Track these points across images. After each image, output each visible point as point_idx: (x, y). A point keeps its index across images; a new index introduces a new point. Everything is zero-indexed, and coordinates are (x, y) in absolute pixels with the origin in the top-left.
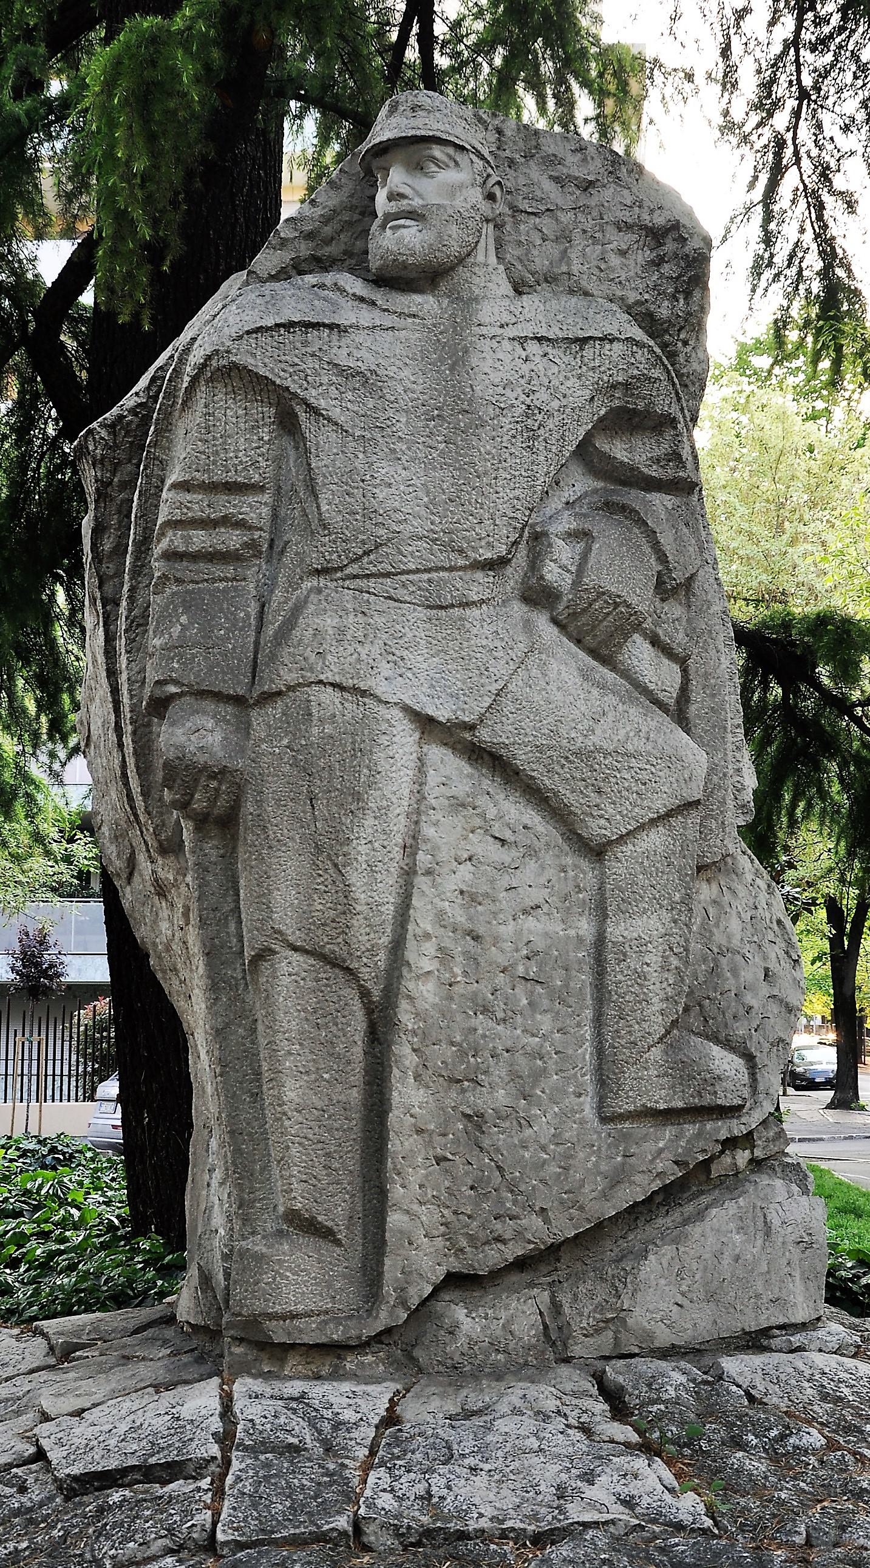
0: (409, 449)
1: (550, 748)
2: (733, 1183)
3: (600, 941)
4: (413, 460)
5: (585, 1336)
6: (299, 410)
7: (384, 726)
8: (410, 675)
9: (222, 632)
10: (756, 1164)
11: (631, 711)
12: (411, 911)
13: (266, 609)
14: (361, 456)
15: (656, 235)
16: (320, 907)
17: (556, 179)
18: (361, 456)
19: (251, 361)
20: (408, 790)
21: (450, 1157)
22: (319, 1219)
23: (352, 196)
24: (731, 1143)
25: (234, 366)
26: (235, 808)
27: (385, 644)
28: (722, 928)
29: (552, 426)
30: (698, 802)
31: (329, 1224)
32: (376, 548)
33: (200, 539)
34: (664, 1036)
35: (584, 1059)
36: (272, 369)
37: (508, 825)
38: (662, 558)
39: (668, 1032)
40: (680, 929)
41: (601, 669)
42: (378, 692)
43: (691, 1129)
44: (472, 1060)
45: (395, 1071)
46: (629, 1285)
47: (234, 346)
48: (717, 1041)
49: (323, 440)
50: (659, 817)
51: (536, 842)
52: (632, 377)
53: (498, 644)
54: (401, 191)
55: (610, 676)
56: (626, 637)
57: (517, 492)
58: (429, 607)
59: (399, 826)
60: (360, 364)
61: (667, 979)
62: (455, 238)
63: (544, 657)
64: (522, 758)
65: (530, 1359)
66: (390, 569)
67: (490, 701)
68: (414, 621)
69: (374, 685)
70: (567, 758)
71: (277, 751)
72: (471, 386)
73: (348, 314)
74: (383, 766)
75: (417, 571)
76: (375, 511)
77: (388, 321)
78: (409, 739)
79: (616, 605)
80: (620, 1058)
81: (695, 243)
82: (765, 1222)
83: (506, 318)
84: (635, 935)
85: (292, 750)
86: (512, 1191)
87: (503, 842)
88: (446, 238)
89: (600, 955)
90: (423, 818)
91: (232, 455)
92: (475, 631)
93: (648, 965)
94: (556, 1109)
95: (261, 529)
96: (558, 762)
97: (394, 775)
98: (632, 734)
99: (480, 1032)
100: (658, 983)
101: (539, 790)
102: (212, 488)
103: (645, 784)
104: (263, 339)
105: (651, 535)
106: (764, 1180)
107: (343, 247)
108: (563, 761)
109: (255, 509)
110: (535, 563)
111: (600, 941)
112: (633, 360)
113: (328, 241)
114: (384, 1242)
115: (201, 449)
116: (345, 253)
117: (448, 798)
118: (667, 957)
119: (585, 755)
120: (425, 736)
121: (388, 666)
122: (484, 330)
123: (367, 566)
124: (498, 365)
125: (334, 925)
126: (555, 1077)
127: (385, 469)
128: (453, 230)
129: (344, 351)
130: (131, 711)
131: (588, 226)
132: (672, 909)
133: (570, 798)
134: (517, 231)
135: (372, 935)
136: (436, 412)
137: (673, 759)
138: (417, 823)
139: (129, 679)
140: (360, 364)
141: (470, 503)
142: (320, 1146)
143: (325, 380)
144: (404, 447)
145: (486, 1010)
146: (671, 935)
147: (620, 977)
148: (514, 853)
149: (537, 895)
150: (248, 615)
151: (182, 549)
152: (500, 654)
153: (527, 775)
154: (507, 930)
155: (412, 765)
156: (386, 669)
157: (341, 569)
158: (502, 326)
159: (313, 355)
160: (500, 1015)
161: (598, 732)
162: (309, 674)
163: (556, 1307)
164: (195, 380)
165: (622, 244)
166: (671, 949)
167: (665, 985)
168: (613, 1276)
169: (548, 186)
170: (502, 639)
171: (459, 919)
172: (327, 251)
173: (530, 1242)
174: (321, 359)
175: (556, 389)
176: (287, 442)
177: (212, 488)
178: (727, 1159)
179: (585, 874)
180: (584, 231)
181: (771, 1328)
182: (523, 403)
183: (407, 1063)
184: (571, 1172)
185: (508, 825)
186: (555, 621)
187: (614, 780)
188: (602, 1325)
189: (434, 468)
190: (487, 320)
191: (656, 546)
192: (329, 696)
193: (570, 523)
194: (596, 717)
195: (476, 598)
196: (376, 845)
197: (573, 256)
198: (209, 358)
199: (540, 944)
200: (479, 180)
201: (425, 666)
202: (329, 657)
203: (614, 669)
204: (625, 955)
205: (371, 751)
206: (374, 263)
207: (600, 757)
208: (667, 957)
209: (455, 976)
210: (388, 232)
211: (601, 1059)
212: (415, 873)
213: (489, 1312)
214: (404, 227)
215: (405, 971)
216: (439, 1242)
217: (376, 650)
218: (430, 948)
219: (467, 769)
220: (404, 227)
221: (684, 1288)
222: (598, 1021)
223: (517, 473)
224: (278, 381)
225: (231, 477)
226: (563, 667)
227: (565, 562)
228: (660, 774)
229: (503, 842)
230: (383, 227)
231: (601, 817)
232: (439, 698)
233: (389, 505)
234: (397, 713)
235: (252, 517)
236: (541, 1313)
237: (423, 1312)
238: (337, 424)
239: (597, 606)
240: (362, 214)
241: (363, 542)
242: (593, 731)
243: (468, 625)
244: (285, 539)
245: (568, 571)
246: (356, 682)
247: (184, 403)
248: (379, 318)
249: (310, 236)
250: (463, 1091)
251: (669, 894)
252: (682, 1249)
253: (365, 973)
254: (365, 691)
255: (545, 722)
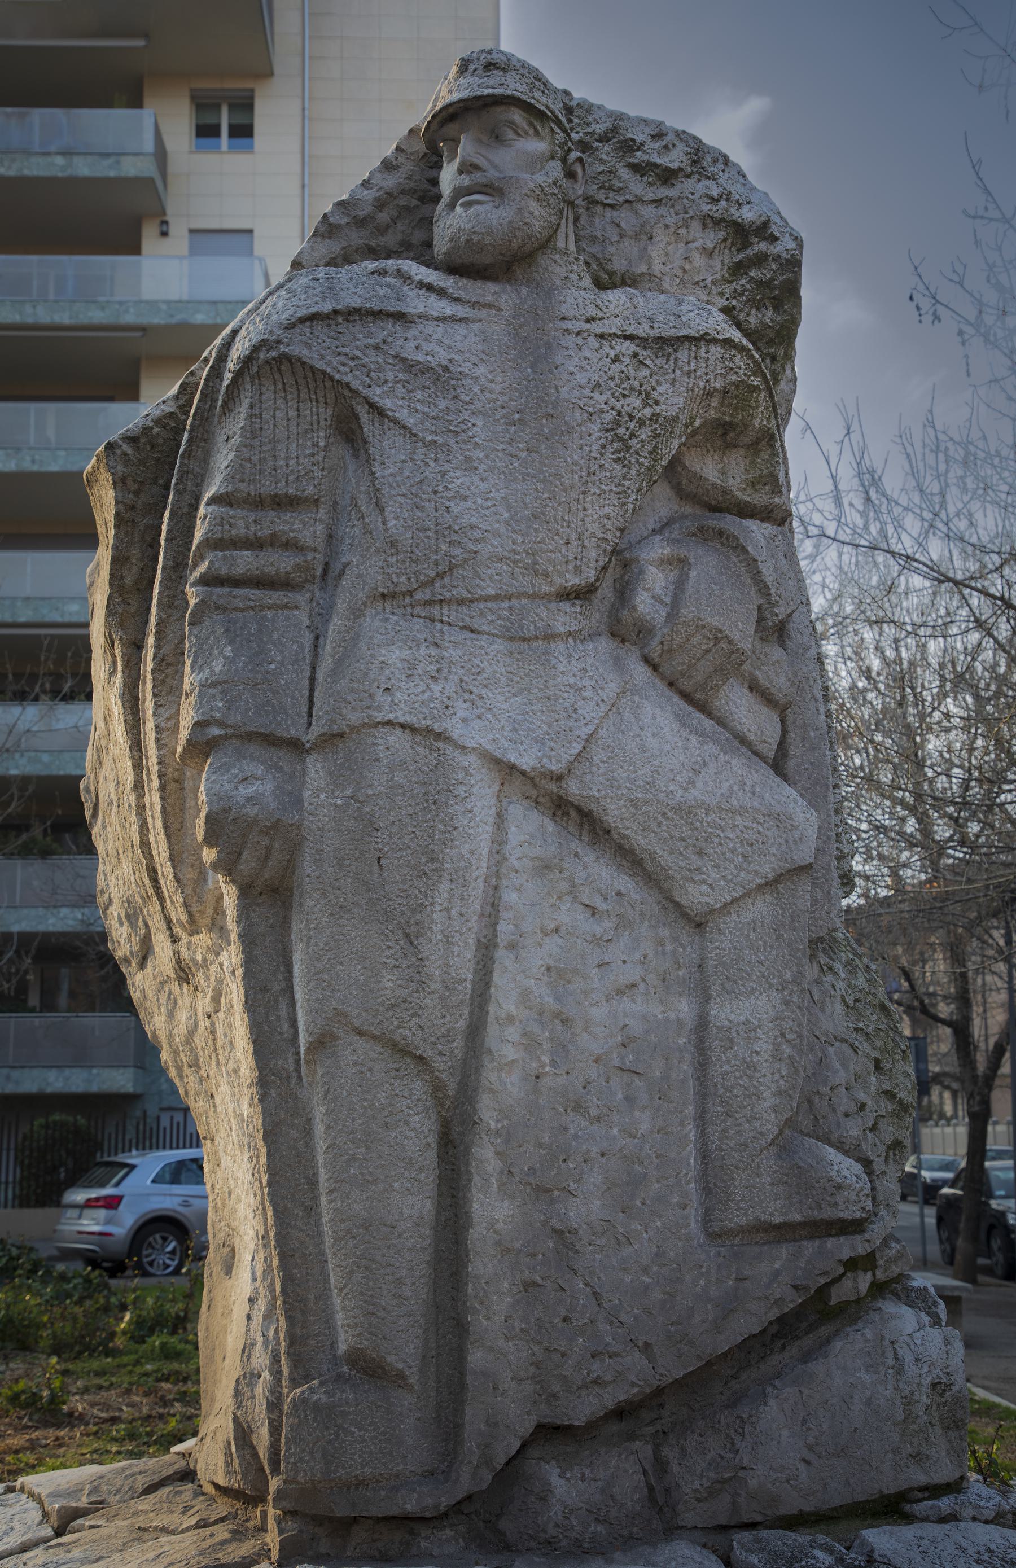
0: (487, 457)
1: (646, 802)
2: (851, 1312)
3: (702, 1024)
4: (491, 470)
5: (699, 1500)
6: (362, 411)
7: (461, 776)
8: (489, 716)
9: (273, 666)
10: (879, 1289)
11: (734, 762)
12: (493, 990)
13: (321, 641)
14: (432, 464)
15: (741, 234)
16: (390, 984)
17: (635, 168)
18: (432, 464)
19: (305, 351)
20: (486, 850)
21: (540, 1281)
22: (389, 1360)
23: (409, 178)
24: (852, 1265)
25: (286, 357)
26: (290, 866)
27: (462, 681)
28: (828, 1012)
29: (644, 436)
30: (810, 865)
31: (400, 1366)
32: (450, 570)
33: (245, 562)
34: (777, 1137)
35: (689, 1164)
36: (330, 362)
37: (599, 891)
38: (764, 590)
39: (781, 1132)
40: (793, 1012)
41: (698, 714)
42: (455, 734)
43: (809, 1247)
44: (563, 1165)
45: (476, 1178)
46: (747, 1436)
47: (285, 336)
48: (830, 1144)
49: (388, 449)
50: (767, 884)
51: (630, 910)
52: (732, 383)
53: (586, 682)
54: (475, 161)
55: (708, 723)
56: (725, 679)
57: (607, 510)
58: (511, 639)
59: (477, 890)
60: (429, 358)
61: (779, 1070)
62: (538, 215)
63: (637, 699)
64: (614, 813)
65: (635, 1530)
66: (466, 594)
67: (580, 747)
68: (492, 656)
69: (449, 726)
70: (665, 814)
71: (339, 802)
72: (556, 387)
73: (417, 303)
74: (462, 821)
75: (497, 598)
76: (450, 527)
77: (461, 311)
78: (488, 791)
79: (717, 641)
80: (728, 1162)
81: (785, 246)
82: (896, 1359)
83: (592, 311)
84: (742, 1018)
85: (357, 801)
86: (611, 1323)
87: (594, 911)
88: (527, 215)
89: (702, 1042)
90: (505, 882)
91: (282, 463)
92: (561, 668)
93: (758, 1053)
94: (659, 1224)
95: (315, 550)
96: (655, 818)
97: (471, 831)
98: (736, 788)
99: (572, 1131)
100: (769, 1075)
101: (632, 852)
102: (258, 503)
103: (752, 845)
104: (319, 327)
105: (751, 564)
106: (889, 1306)
107: (399, 237)
108: (660, 818)
109: (307, 528)
110: (624, 592)
111: (702, 1024)
112: (731, 365)
113: (382, 230)
114: (463, 1386)
115: (247, 456)
116: (401, 244)
117: (532, 859)
118: (779, 1045)
119: (685, 811)
120: (505, 788)
121: (465, 706)
122: (568, 325)
123: (440, 591)
124: (585, 363)
125: (407, 1005)
126: (657, 1186)
127: (459, 480)
128: (533, 205)
129: (411, 344)
130: (159, 763)
131: (670, 220)
132: (783, 989)
133: (667, 859)
134: (592, 224)
135: (448, 1018)
136: (517, 416)
137: (780, 820)
138: (496, 888)
139: (157, 726)
140: (429, 358)
141: (556, 520)
142: (389, 1270)
143: (390, 376)
144: (481, 455)
145: (578, 1106)
146: (783, 1019)
147: (726, 1067)
148: (608, 924)
149: (634, 973)
150: (302, 647)
151: (224, 571)
152: (588, 694)
153: (619, 834)
154: (598, 1013)
155: (491, 820)
156: (461, 709)
157: (411, 593)
158: (588, 321)
159: (377, 348)
160: (594, 1112)
161: (699, 785)
162: (376, 714)
163: (661, 1465)
164: (238, 375)
165: (708, 242)
166: (783, 1035)
167: (777, 1077)
168: (728, 1425)
169: (625, 173)
170: (591, 678)
171: (546, 999)
172: (382, 241)
173: (633, 1384)
174: (385, 353)
175: (648, 395)
176: (340, 450)
177: (258, 503)
178: (848, 1283)
179: (684, 948)
180: (667, 226)
181: (912, 1489)
182: (613, 408)
183: (490, 1169)
184: (678, 1298)
185: (599, 891)
186: (647, 660)
187: (717, 840)
188: (718, 1486)
189: (516, 480)
190: (571, 313)
191: (757, 576)
192: (396, 739)
193: (662, 547)
194: (696, 767)
195: (562, 629)
196: (453, 912)
197: (654, 254)
198: (256, 349)
199: (636, 1028)
200: (560, 153)
201: (505, 706)
202: (398, 694)
203: (709, 715)
204: (731, 1041)
205: (446, 803)
206: (441, 246)
207: (701, 813)
208: (779, 1045)
209: (543, 1066)
210: (459, 209)
211: (707, 1164)
212: (496, 945)
213: (587, 1471)
214: (478, 202)
215: (486, 1060)
216: (529, 1387)
217: (451, 688)
218: (513, 1033)
219: (551, 827)
220: (478, 202)
221: (811, 1440)
222: (702, 1119)
223: (606, 488)
224: (337, 377)
225: (281, 488)
226: (658, 711)
227: (658, 591)
228: (768, 833)
229: (594, 911)
230: (451, 206)
231: (703, 882)
232: (522, 743)
233: (465, 520)
234: (472, 761)
235: (305, 537)
236: (645, 1472)
237: (511, 1473)
238: (404, 427)
239: (695, 641)
240: (422, 199)
241: (437, 563)
242: (694, 783)
243: (553, 661)
244: (344, 560)
245: (662, 602)
246: (429, 722)
247: (225, 403)
248: (448, 308)
249: (360, 223)
250: (553, 1201)
251: (779, 971)
252: (806, 1392)
253: (439, 1064)
254: (440, 734)
255: (640, 773)
